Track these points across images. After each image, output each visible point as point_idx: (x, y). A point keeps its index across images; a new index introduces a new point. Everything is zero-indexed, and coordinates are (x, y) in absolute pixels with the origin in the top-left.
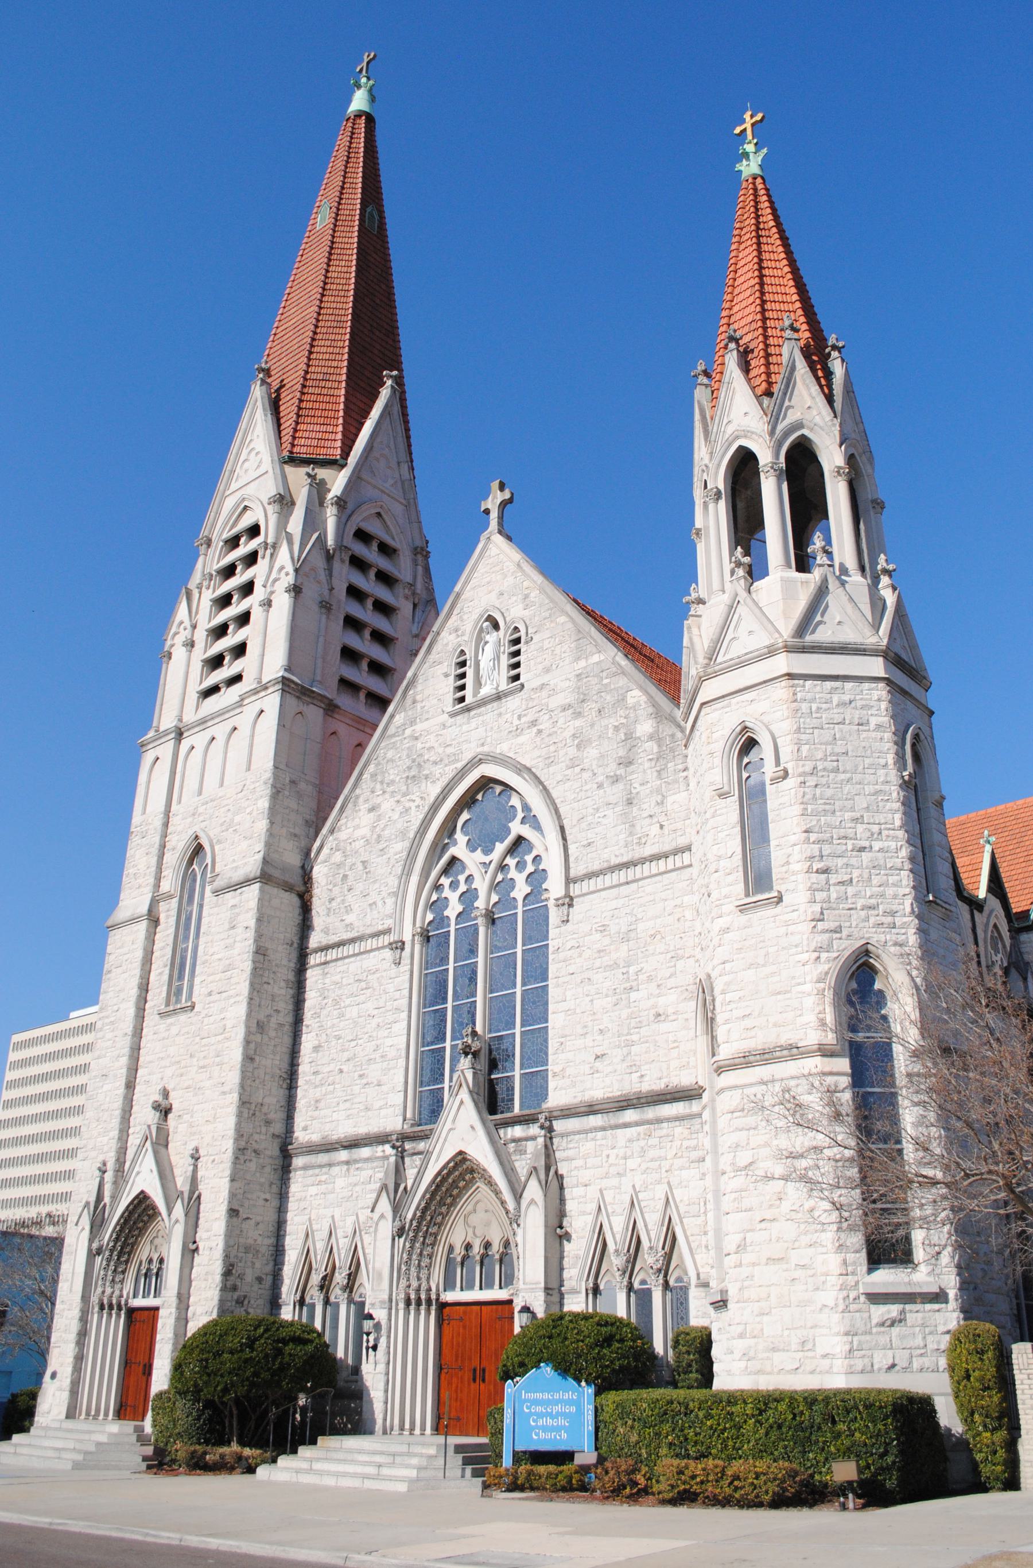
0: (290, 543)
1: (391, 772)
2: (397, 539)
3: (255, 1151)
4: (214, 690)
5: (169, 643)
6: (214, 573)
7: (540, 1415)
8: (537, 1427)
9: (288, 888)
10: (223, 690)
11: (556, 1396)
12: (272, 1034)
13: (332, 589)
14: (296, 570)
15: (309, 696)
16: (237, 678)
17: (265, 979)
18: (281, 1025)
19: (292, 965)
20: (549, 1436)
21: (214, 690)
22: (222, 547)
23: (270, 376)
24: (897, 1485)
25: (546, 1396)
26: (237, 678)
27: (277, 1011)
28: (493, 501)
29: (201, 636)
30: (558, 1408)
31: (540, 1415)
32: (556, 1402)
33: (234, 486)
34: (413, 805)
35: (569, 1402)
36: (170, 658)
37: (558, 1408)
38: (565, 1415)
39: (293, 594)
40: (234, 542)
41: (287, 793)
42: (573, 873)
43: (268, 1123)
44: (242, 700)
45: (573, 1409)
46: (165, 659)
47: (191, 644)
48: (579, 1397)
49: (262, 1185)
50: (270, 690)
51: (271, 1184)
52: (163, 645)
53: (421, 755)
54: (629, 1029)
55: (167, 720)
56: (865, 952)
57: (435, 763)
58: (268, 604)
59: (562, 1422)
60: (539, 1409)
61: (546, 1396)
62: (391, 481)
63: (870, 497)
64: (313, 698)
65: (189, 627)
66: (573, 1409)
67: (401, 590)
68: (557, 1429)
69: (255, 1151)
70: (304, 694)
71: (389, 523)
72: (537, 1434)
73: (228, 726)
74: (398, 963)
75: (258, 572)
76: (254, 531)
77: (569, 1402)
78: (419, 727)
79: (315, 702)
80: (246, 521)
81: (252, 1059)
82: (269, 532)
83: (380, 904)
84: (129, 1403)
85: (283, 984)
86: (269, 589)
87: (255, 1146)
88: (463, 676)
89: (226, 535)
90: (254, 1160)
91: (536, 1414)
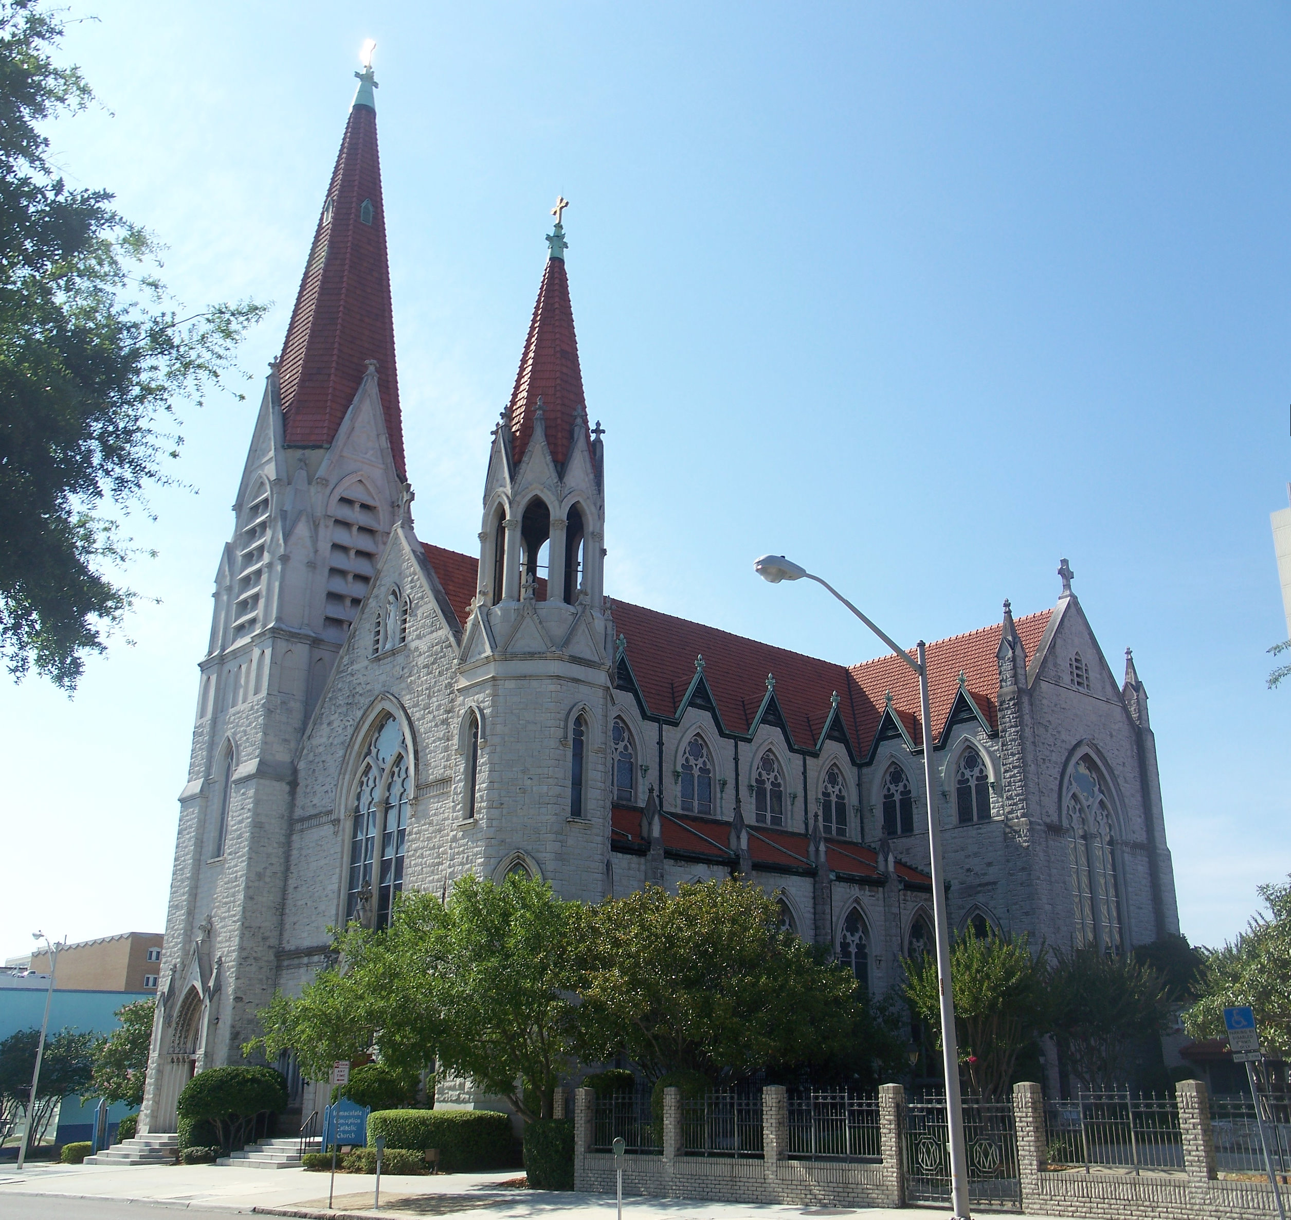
1: (340, 698)
2: (377, 499)
3: (255, 958)
7: (342, 1125)
9: (279, 778)
11: (351, 1114)
12: (267, 880)
13: (316, 551)
15: (297, 638)
17: (262, 844)
18: (275, 873)
19: (283, 832)
20: (346, 1136)
25: (346, 1114)
27: (272, 864)
30: (350, 1121)
31: (342, 1125)
34: (349, 724)
38: (354, 1124)
41: (278, 711)
43: (265, 939)
45: (359, 1121)
48: (362, 1114)
49: (261, 980)
50: (267, 637)
51: (268, 978)
53: (355, 688)
54: (437, 889)
57: (361, 695)
61: (346, 1114)
62: (371, 452)
63: (229, 733)
64: (300, 638)
67: (380, 538)
68: (350, 1132)
69: (255, 958)
70: (292, 637)
71: (369, 487)
72: (340, 1135)
74: (336, 833)
77: (358, 1117)
78: (355, 667)
79: (302, 641)
81: (252, 898)
83: (330, 791)
85: (275, 845)
87: (255, 955)
88: (378, 633)
90: (254, 964)
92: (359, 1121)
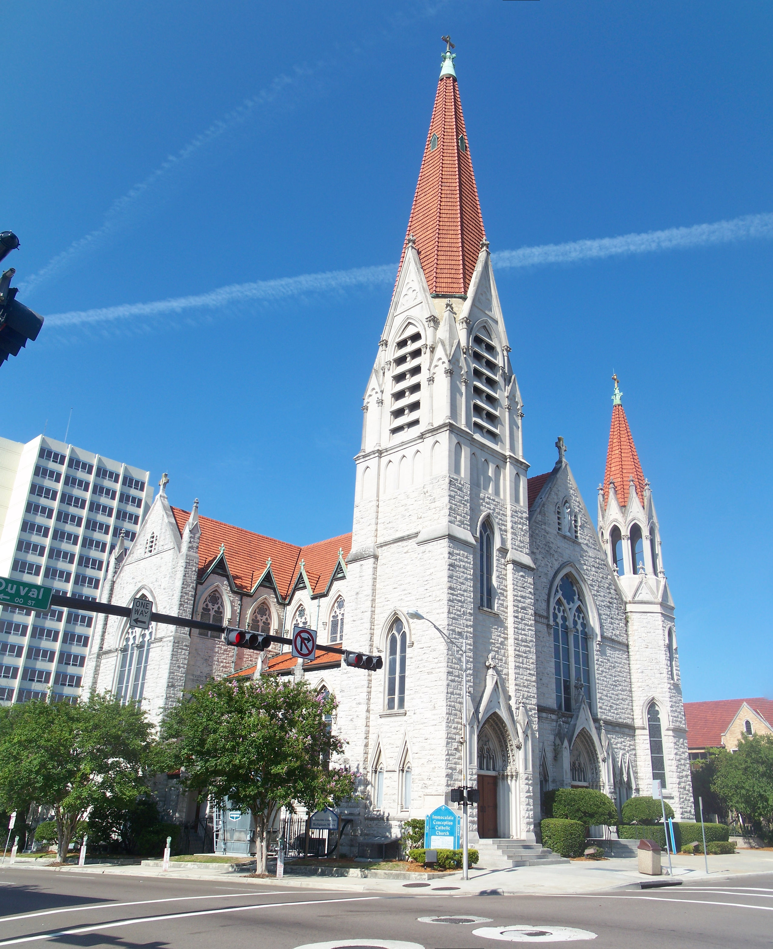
0: (443, 345)
4: (400, 429)
5: (366, 401)
6: (392, 361)
7: (440, 825)
8: (438, 830)
10: (406, 429)
14: (449, 361)
16: (416, 422)
21: (400, 429)
22: (396, 346)
23: (415, 244)
24: (113, 840)
25: (442, 818)
26: (416, 422)
28: (163, 480)
29: (388, 398)
31: (440, 825)
32: (445, 820)
33: (398, 312)
35: (450, 821)
36: (367, 410)
37: (445, 823)
38: (449, 826)
39: (449, 374)
40: (402, 344)
42: (106, 647)
44: (423, 435)
46: (365, 410)
47: (381, 402)
52: (363, 403)
55: (369, 445)
56: (653, 699)
58: (431, 380)
59: (448, 828)
60: (439, 823)
65: (379, 392)
66: (452, 823)
73: (415, 448)
75: (423, 360)
76: (416, 337)
77: (450, 821)
80: (411, 331)
82: (427, 338)
84: (462, 806)
86: (432, 372)
89: (398, 340)
91: (438, 825)
92: (452, 823)
